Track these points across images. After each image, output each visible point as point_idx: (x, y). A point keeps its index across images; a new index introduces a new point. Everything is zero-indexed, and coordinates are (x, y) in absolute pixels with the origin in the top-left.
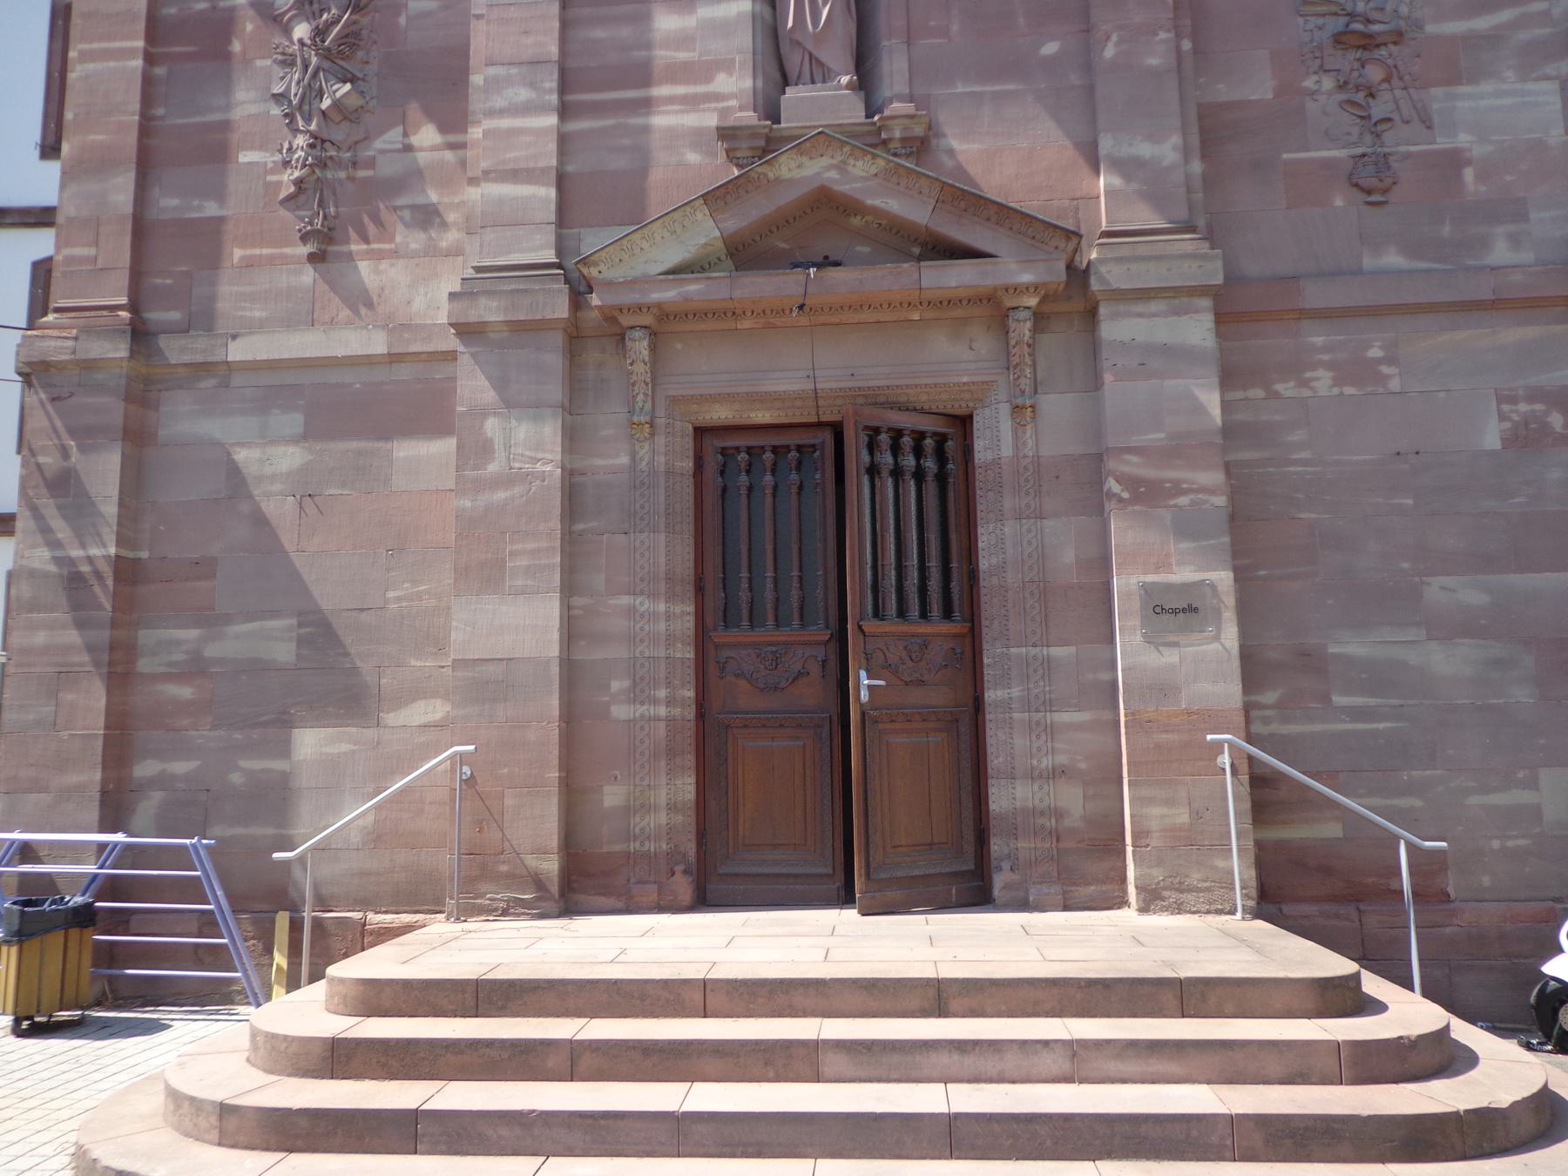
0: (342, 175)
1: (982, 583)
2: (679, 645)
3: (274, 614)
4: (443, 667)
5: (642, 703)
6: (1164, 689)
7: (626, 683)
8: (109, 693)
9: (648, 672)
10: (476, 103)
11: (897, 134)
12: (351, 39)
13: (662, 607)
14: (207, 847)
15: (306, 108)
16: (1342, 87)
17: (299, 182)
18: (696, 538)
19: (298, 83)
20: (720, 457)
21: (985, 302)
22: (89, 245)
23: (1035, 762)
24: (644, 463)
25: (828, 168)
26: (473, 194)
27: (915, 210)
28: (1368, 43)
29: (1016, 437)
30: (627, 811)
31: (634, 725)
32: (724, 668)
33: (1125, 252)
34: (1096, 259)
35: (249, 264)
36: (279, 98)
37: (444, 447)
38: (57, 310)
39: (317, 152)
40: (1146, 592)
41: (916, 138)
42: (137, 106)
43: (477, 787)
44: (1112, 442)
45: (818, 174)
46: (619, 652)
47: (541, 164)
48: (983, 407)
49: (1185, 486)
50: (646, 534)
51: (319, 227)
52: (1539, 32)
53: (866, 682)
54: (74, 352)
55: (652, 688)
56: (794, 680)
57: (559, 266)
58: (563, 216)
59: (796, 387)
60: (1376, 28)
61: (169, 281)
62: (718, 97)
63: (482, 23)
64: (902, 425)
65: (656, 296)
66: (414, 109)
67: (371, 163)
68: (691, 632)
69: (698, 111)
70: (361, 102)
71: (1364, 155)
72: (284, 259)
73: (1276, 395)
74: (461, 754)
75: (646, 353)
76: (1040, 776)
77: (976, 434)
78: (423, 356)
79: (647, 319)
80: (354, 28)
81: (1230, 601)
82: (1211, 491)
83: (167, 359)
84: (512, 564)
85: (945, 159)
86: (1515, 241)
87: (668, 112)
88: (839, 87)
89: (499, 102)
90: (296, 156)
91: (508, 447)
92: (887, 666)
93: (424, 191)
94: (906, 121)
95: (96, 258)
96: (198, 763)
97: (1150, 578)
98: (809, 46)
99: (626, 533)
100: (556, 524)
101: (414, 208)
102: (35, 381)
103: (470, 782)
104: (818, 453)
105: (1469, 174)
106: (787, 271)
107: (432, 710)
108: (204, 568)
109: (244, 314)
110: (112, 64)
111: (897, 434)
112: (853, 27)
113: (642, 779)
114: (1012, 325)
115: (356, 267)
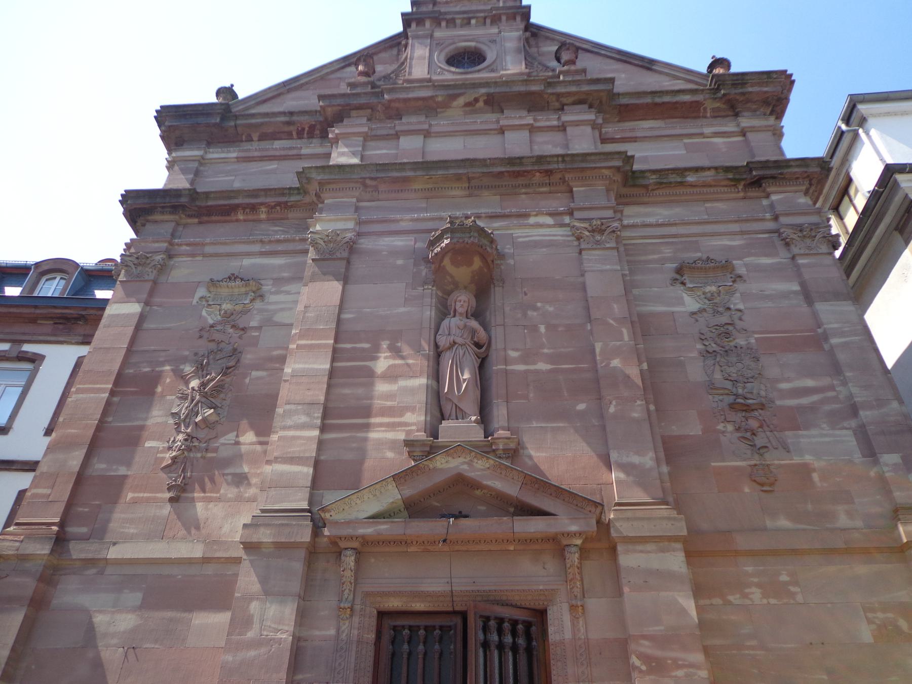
0: (199, 455)
10: (277, 422)
11: (501, 447)
15: (188, 420)
16: (738, 429)
17: (174, 459)
19: (187, 407)
20: (392, 632)
21: (551, 541)
24: (344, 635)
26: (268, 469)
29: (573, 625)
33: (629, 514)
35: (135, 502)
36: (174, 415)
37: (222, 618)
38: (17, 524)
39: (188, 443)
42: (99, 416)
47: (307, 455)
49: (680, 663)
57: (309, 511)
59: (439, 589)
60: (750, 401)
61: (86, 510)
62: (406, 424)
64: (503, 615)
65: (361, 531)
66: (244, 423)
67: (216, 450)
70: (217, 419)
71: (756, 465)
72: (155, 500)
73: (730, 603)
75: (352, 564)
77: (549, 622)
78: (222, 559)
79: (355, 544)
80: (221, 383)
83: (71, 555)
85: (527, 460)
88: (471, 422)
89: (289, 422)
91: (262, 621)
93: (241, 466)
98: (456, 401)
104: (452, 632)
105: (815, 476)
110: (92, 395)
111: (500, 621)
112: (478, 393)
114: (567, 555)
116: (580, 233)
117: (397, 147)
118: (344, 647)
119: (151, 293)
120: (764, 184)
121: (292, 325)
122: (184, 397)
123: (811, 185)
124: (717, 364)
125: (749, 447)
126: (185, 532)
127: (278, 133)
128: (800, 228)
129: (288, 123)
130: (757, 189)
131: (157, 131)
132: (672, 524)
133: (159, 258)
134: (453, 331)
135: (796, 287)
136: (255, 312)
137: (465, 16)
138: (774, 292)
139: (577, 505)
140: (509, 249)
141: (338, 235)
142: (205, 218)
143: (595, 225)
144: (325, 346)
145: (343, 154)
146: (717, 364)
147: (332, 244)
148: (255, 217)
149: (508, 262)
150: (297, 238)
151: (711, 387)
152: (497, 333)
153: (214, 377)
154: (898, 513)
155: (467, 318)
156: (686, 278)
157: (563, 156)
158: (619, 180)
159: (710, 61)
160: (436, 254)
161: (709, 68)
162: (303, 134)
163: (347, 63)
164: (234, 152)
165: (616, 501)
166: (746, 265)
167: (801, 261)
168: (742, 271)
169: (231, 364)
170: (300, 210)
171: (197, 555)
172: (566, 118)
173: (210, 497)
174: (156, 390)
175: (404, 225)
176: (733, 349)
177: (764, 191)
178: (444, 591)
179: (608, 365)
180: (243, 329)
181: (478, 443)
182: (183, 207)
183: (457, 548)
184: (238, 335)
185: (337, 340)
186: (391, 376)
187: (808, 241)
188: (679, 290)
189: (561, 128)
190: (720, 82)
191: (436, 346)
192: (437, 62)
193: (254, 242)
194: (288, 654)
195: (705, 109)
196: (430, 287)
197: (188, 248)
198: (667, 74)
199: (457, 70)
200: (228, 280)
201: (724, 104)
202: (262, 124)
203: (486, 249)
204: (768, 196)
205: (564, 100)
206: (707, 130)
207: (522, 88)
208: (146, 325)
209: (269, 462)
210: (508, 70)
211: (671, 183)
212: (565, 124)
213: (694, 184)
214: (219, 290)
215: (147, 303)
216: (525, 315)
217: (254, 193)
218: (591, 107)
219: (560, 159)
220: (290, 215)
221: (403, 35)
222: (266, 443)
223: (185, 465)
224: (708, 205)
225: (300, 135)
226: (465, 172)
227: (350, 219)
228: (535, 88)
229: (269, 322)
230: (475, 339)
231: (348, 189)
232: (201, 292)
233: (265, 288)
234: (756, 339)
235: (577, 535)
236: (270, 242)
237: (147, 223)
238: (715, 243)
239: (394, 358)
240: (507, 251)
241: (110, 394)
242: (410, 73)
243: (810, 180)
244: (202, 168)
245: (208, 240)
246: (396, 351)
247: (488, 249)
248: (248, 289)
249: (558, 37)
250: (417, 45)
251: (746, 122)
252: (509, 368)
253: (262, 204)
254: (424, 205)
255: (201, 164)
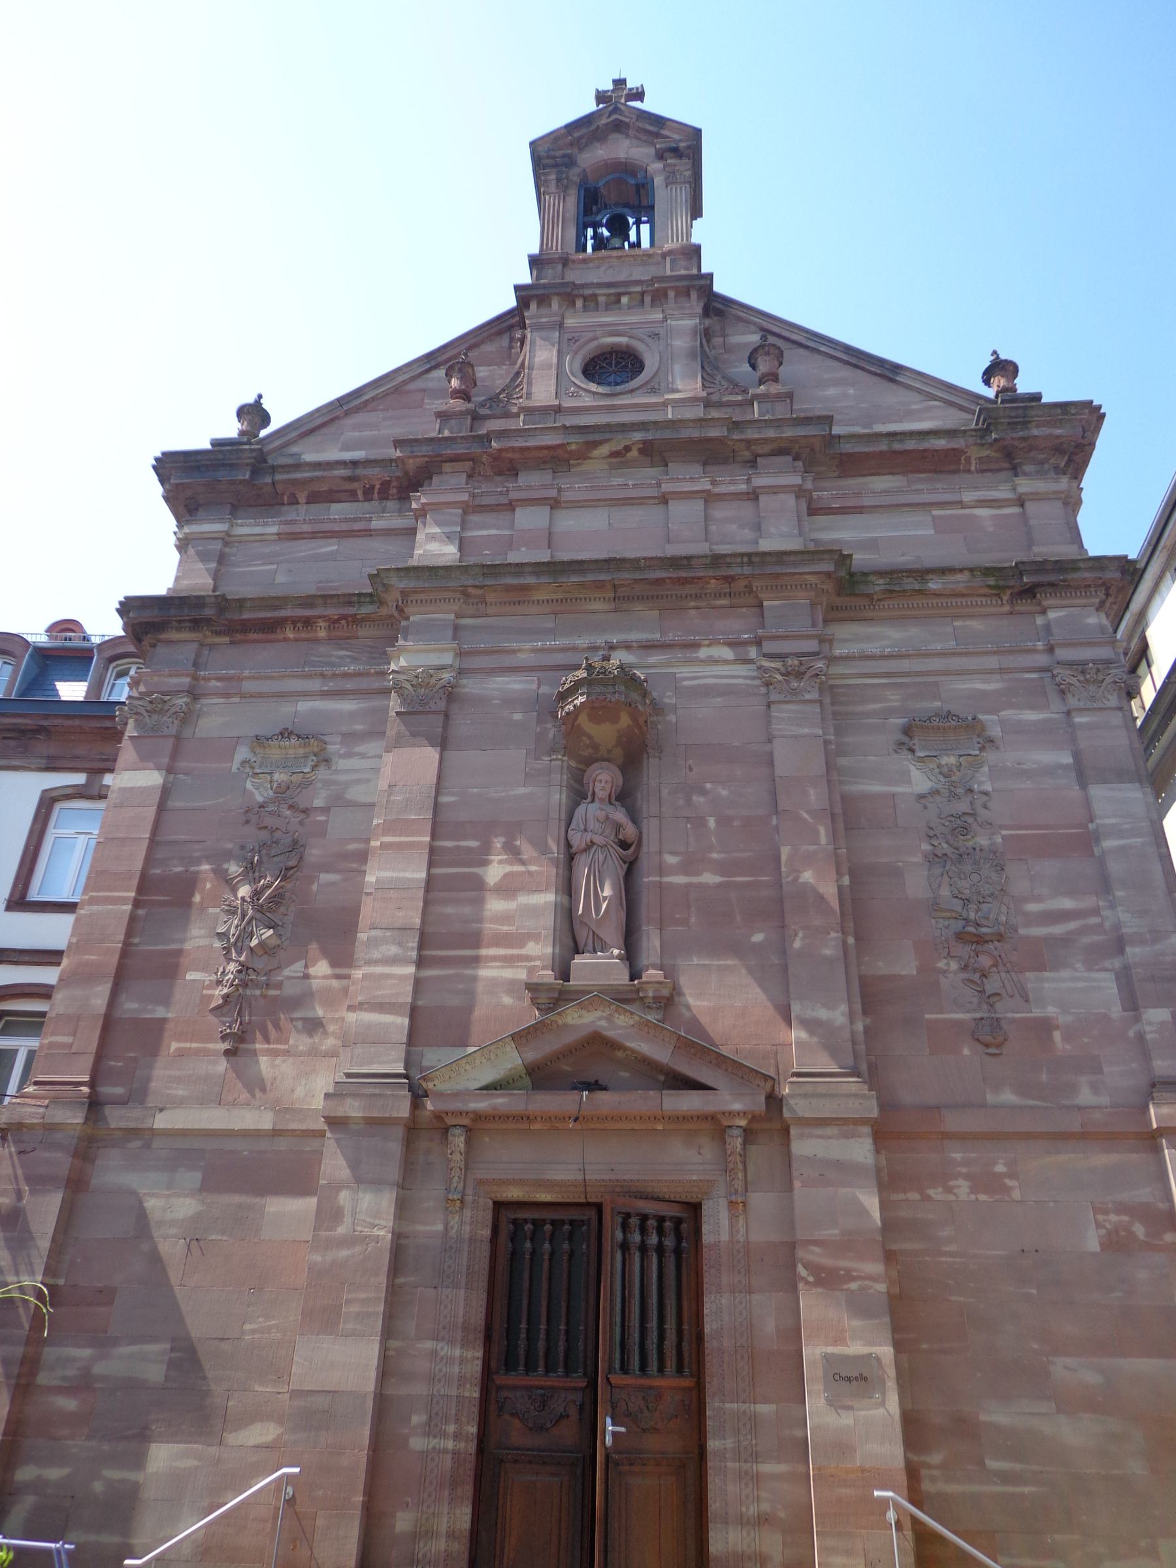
0: (258, 992)
1: (706, 1345)
2: (468, 1386)
3: (154, 1339)
4: (279, 1393)
5: (435, 1437)
6: (842, 1447)
7: (424, 1418)
8: (12, 1401)
9: (442, 1408)
10: (360, 953)
11: (650, 994)
12: (277, 899)
13: (457, 1352)
14: (68, 1552)
15: (239, 944)
16: (965, 968)
17: (226, 997)
18: (488, 1293)
19: (237, 927)
20: (511, 1226)
21: (709, 1119)
22: (69, 1034)
23: (744, 1509)
24: (454, 1231)
25: (600, 1018)
26: (352, 1017)
27: (661, 1053)
28: (980, 940)
29: (731, 1226)
30: (415, 1536)
31: (427, 1456)
32: (502, 1406)
33: (809, 1089)
34: (788, 1094)
35: (181, 1054)
36: (222, 936)
37: (306, 1205)
38: (36, 1083)
39: (242, 976)
40: (827, 1361)
41: (663, 997)
42: (122, 938)
43: (296, 1507)
44: (800, 1235)
45: (593, 1022)
46: (420, 1389)
47: (400, 1000)
48: (708, 1199)
49: (854, 1274)
50: (451, 1289)
51: (236, 1030)
52: (1096, 938)
53: (610, 1428)
54: (43, 1118)
55: (444, 1423)
56: (557, 1422)
57: (406, 1076)
58: (413, 1037)
59: (571, 1177)
60: (984, 930)
61: (120, 1064)
62: (528, 958)
63: (370, 898)
64: (647, 1211)
65: (474, 1106)
66: (314, 947)
67: (279, 986)
68: (478, 1375)
69: (513, 967)
70: (279, 942)
71: (982, 1019)
72: (207, 1053)
73: (928, 1198)
74: (288, 1475)
75: (462, 1146)
76: (748, 1523)
77: (704, 1219)
78: (298, 1132)
79: (465, 1121)
80: (281, 891)
81: (891, 1372)
82: (873, 1279)
83: (108, 1124)
84: (346, 1310)
85: (684, 1011)
86: (1095, 1088)
87: (492, 967)
88: (612, 957)
89: (376, 955)
90: (227, 978)
91: (354, 1214)
92: (628, 1414)
93: (314, 1008)
94: (656, 985)
95: (72, 1045)
96: (70, 1470)
97: (830, 1350)
98: (593, 927)
99: (435, 1288)
100: (383, 1279)
101: (304, 1020)
102: (9, 1137)
103: (291, 1502)
104: (584, 1228)
105: (1057, 1036)
106: (568, 1092)
107: (261, 1433)
108: (106, 1295)
109: (171, 1092)
110: (110, 907)
111: (644, 1218)
112: (623, 915)
113: (429, 1507)
114: (728, 1140)
115: (258, 1061)
116: (770, 676)
117: (512, 527)
118: (455, 1246)
119: (175, 754)
120: (1038, 595)
121: (373, 805)
122: (232, 911)
123: (1107, 595)
124: (945, 875)
125: (977, 993)
126: (248, 1095)
127: (338, 491)
128: (1080, 667)
129: (351, 479)
130: (1029, 601)
131: (158, 489)
132: (861, 1104)
133: (181, 701)
134: (591, 826)
135: (1067, 759)
136: (319, 785)
137: (612, 291)
138: (1035, 766)
139: (742, 1077)
140: (669, 697)
141: (432, 676)
142: (239, 637)
143: (791, 666)
144: (418, 845)
145: (432, 538)
146: (945, 875)
147: (423, 690)
148: (311, 635)
149: (668, 718)
150: (373, 670)
151: (935, 906)
152: (650, 827)
153: (270, 882)
154: (1159, 1086)
155: (610, 803)
156: (916, 742)
157: (749, 555)
158: (830, 590)
159: (986, 363)
160: (567, 714)
161: (984, 374)
162: (373, 494)
163: (433, 363)
164: (273, 524)
165: (794, 1070)
166: (1002, 722)
167: (1078, 719)
168: (996, 732)
169: (291, 864)
170: (374, 625)
171: (266, 1127)
172: (760, 481)
173: (277, 1049)
174: (193, 899)
175: (523, 658)
176: (971, 851)
177: (1039, 604)
178: (576, 1180)
179: (796, 879)
180: (305, 811)
181: (620, 988)
182: (208, 621)
183: (593, 1126)
184: (299, 819)
185: (434, 836)
186: (507, 889)
187: (1092, 688)
188: (905, 761)
189: (752, 496)
190: (990, 421)
191: (569, 845)
192: (570, 375)
193: (311, 675)
194: (388, 1254)
195: (968, 460)
196: (560, 757)
197: (219, 684)
198: (919, 391)
199: (600, 389)
200: (280, 737)
201: (996, 451)
202: (312, 480)
203: (636, 707)
204: (1044, 612)
205: (759, 449)
206: (968, 497)
207: (695, 434)
208: (171, 804)
209: (351, 1008)
210: (677, 391)
211: (905, 591)
212: (757, 490)
213: (937, 592)
214: (268, 751)
215: (170, 770)
216: (688, 801)
217: (308, 601)
218: (796, 458)
219: (746, 559)
220: (362, 632)
221: (516, 312)
222: (348, 977)
223: (240, 1008)
224: (957, 623)
225: (368, 494)
226: (610, 578)
227: (446, 650)
228: (713, 433)
229: (339, 801)
230: (620, 837)
231: (442, 601)
232: (242, 753)
233: (331, 748)
234: (1003, 838)
235: (742, 1115)
236: (334, 675)
237: (159, 644)
238: (963, 687)
239: (511, 864)
240: (666, 700)
241: (133, 905)
242: (529, 395)
243: (1107, 589)
244: (227, 550)
245: (246, 673)
246: (514, 853)
247: (640, 707)
248: (307, 750)
249: (757, 320)
250: (539, 342)
251: (1025, 485)
252: (666, 879)
253: (320, 617)
254: (551, 625)
255: (226, 544)
